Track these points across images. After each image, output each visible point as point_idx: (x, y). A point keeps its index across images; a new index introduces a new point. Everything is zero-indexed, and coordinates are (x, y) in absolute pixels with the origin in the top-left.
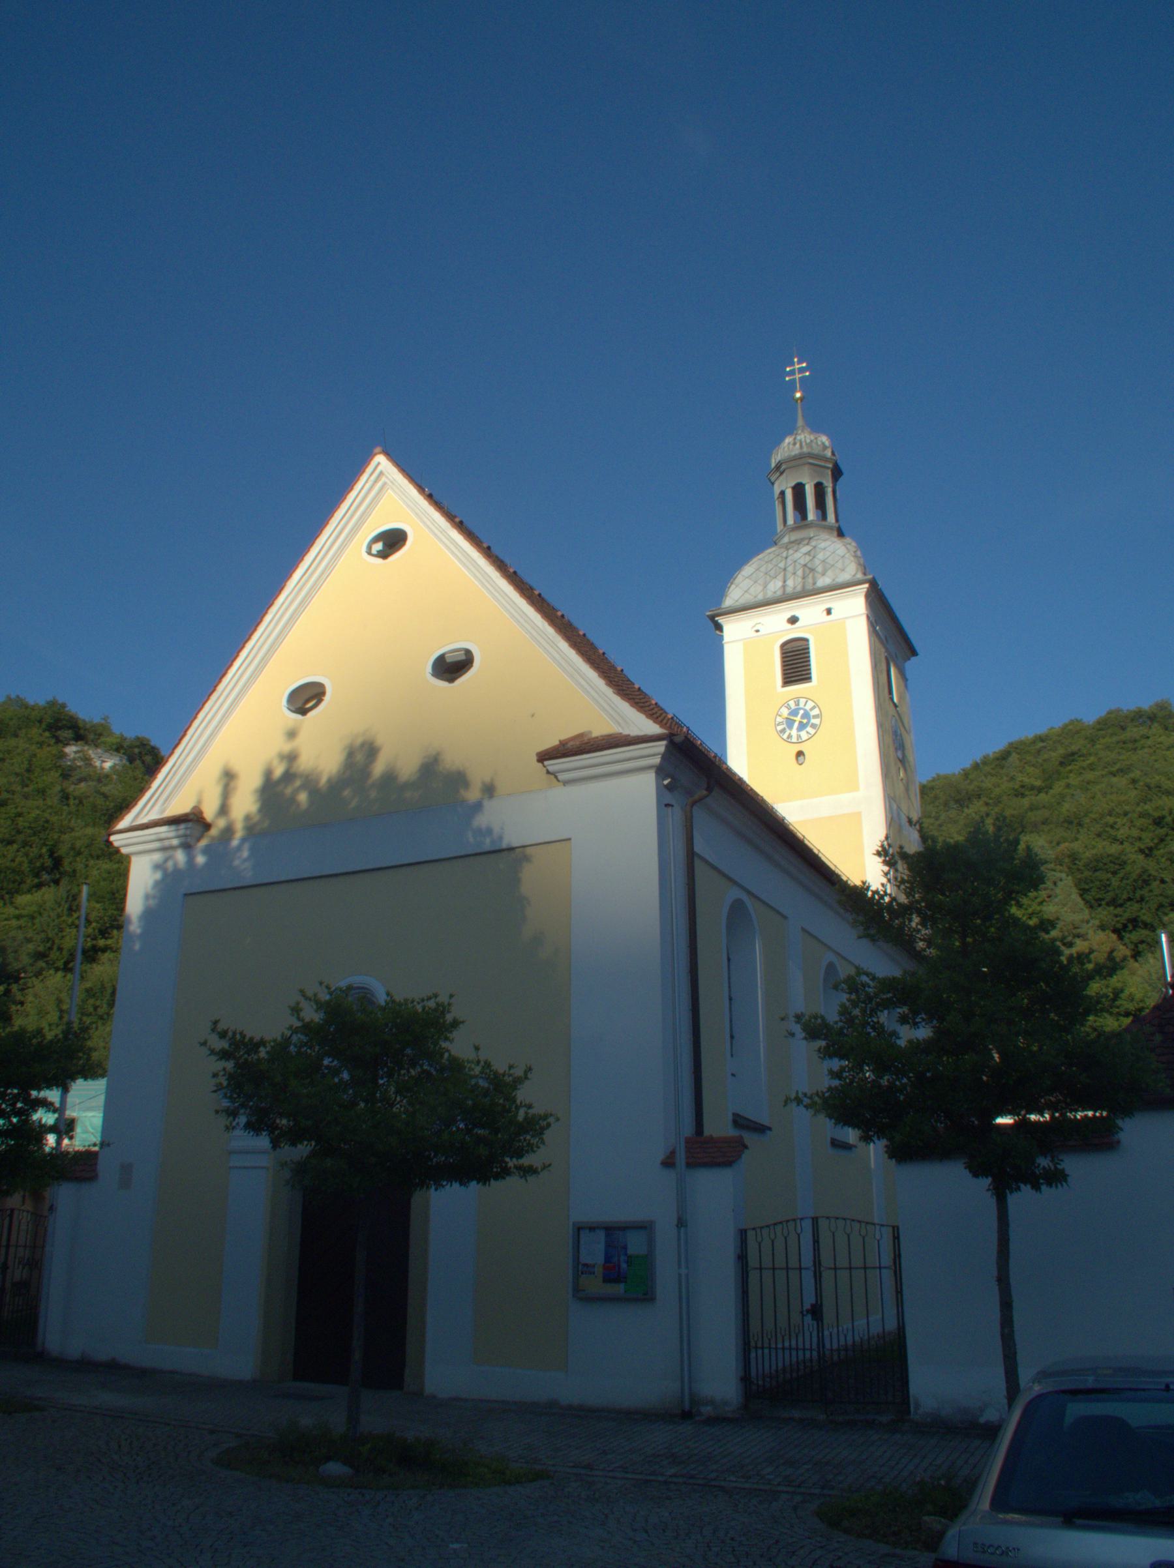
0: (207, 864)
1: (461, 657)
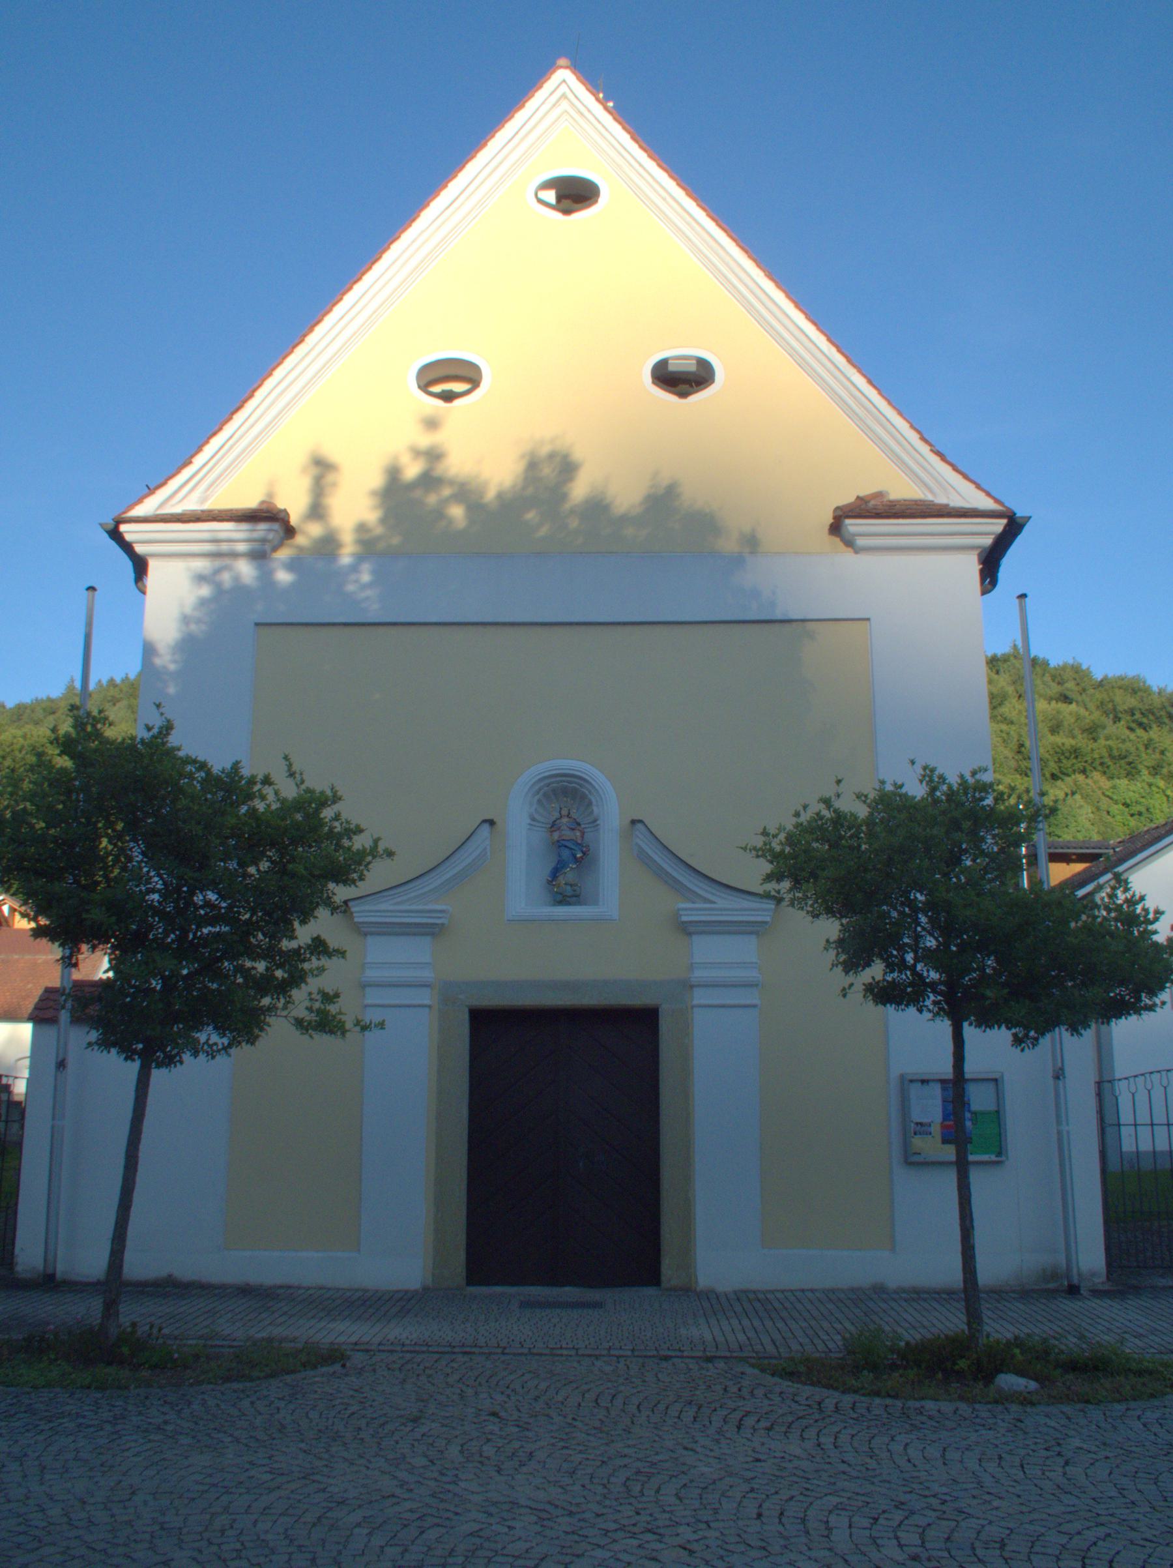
0: (293, 586)
1: (692, 367)
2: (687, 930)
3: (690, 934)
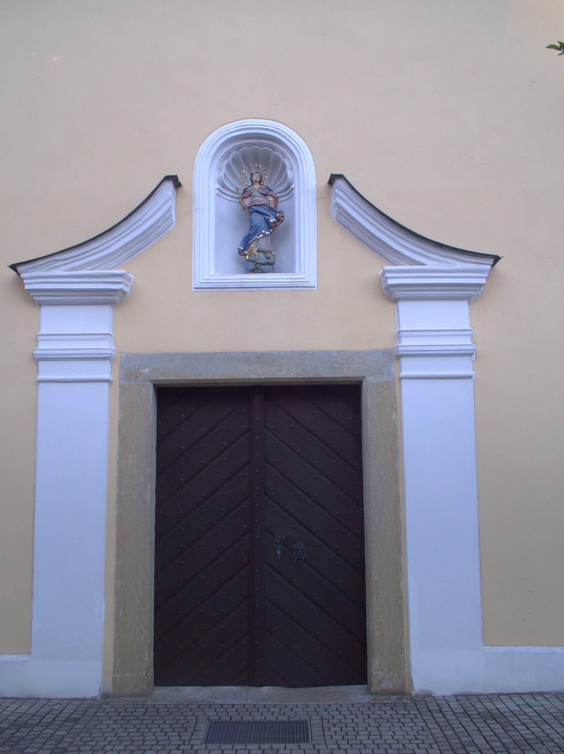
2: (392, 295)
3: (396, 301)
